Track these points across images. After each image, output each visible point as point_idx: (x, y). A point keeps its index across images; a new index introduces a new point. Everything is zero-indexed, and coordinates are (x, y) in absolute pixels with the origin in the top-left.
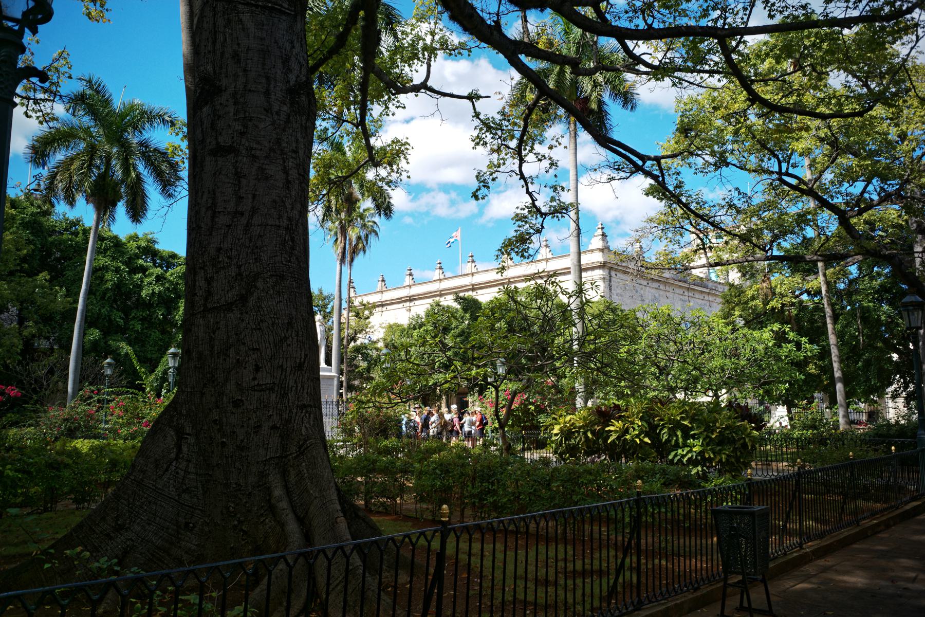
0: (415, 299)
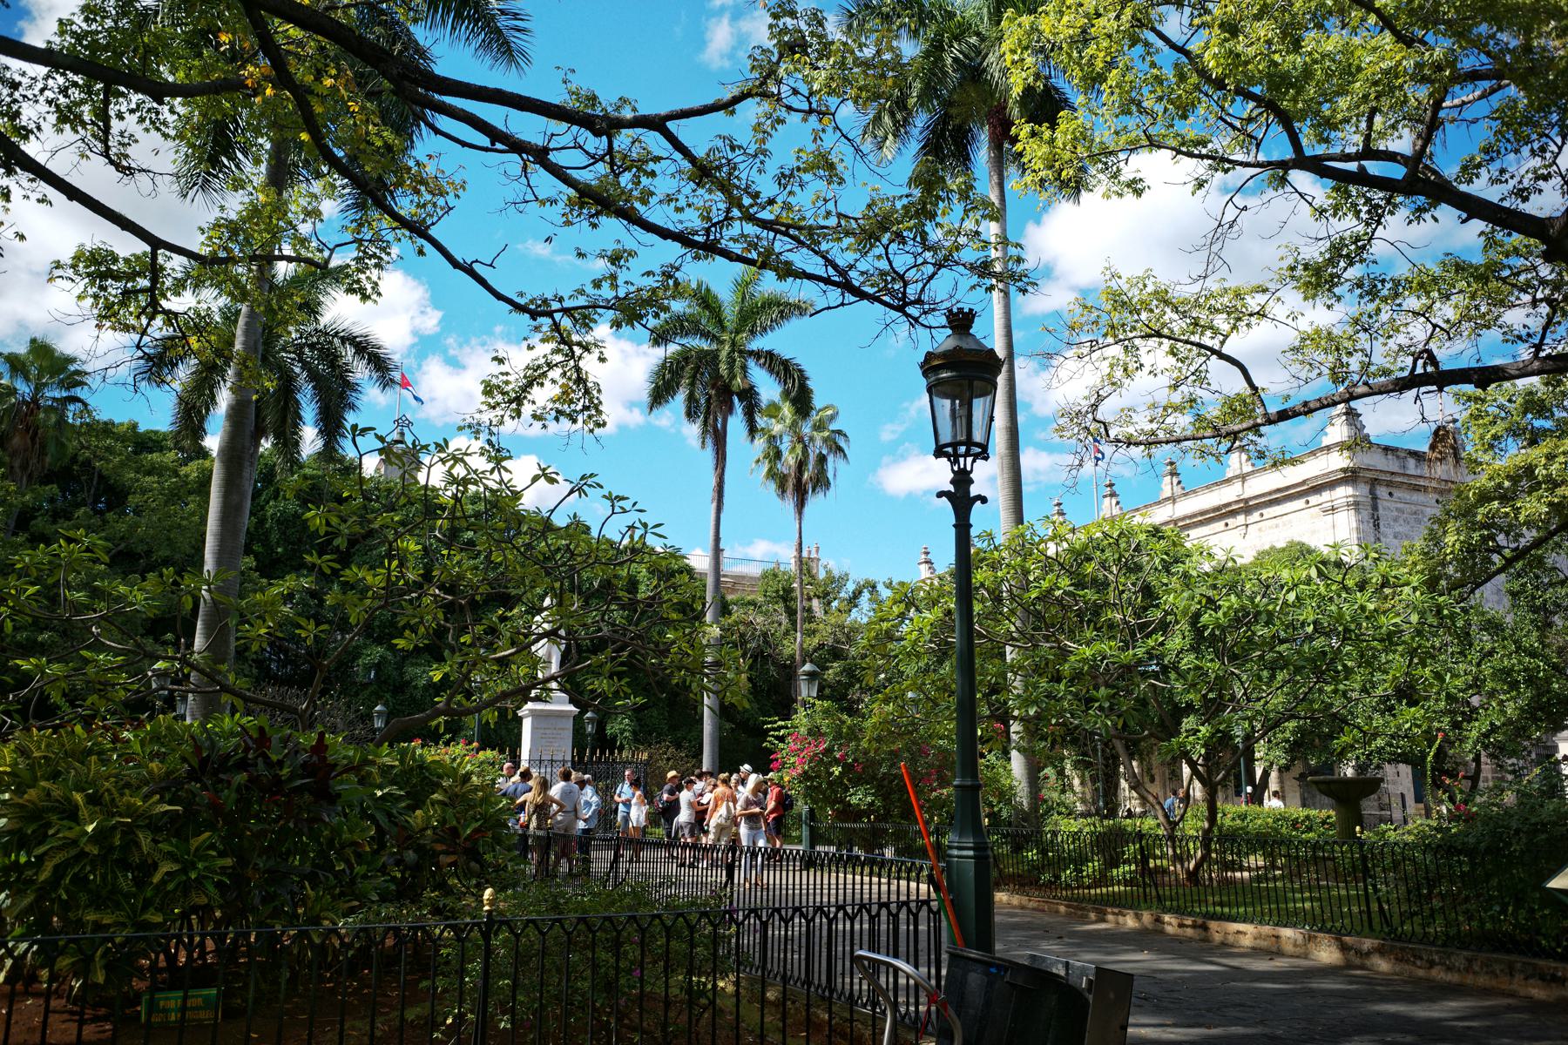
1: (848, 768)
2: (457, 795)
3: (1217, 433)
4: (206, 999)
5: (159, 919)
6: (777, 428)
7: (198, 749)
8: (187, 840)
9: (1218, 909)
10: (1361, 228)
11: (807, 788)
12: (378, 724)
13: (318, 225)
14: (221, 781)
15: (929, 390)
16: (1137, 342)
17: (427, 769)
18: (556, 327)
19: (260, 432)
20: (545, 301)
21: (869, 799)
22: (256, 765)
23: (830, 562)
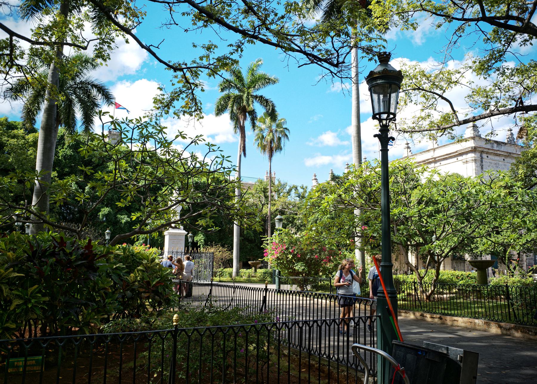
0: (439, 161)
1: (294, 256)
2: (149, 267)
3: (439, 128)
4: (37, 361)
5: (14, 326)
6: (263, 126)
7: (31, 247)
8: (27, 289)
9: (443, 311)
10: (501, 48)
11: (278, 264)
12: (107, 237)
13: (82, 32)
14: (43, 262)
15: (370, 89)
16: (411, 91)
17: (135, 256)
18: (184, 76)
19: (59, 122)
20: (179, 65)
21: (303, 268)
22: (59, 254)
23: (280, 177)
